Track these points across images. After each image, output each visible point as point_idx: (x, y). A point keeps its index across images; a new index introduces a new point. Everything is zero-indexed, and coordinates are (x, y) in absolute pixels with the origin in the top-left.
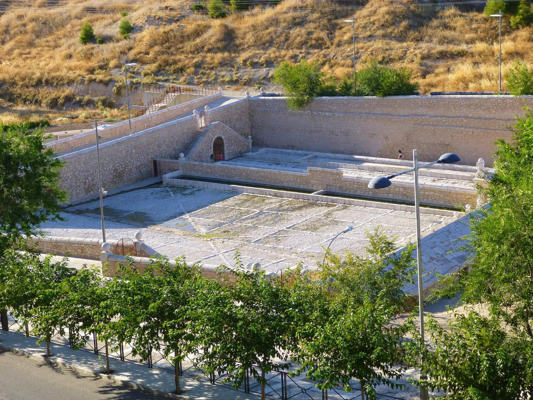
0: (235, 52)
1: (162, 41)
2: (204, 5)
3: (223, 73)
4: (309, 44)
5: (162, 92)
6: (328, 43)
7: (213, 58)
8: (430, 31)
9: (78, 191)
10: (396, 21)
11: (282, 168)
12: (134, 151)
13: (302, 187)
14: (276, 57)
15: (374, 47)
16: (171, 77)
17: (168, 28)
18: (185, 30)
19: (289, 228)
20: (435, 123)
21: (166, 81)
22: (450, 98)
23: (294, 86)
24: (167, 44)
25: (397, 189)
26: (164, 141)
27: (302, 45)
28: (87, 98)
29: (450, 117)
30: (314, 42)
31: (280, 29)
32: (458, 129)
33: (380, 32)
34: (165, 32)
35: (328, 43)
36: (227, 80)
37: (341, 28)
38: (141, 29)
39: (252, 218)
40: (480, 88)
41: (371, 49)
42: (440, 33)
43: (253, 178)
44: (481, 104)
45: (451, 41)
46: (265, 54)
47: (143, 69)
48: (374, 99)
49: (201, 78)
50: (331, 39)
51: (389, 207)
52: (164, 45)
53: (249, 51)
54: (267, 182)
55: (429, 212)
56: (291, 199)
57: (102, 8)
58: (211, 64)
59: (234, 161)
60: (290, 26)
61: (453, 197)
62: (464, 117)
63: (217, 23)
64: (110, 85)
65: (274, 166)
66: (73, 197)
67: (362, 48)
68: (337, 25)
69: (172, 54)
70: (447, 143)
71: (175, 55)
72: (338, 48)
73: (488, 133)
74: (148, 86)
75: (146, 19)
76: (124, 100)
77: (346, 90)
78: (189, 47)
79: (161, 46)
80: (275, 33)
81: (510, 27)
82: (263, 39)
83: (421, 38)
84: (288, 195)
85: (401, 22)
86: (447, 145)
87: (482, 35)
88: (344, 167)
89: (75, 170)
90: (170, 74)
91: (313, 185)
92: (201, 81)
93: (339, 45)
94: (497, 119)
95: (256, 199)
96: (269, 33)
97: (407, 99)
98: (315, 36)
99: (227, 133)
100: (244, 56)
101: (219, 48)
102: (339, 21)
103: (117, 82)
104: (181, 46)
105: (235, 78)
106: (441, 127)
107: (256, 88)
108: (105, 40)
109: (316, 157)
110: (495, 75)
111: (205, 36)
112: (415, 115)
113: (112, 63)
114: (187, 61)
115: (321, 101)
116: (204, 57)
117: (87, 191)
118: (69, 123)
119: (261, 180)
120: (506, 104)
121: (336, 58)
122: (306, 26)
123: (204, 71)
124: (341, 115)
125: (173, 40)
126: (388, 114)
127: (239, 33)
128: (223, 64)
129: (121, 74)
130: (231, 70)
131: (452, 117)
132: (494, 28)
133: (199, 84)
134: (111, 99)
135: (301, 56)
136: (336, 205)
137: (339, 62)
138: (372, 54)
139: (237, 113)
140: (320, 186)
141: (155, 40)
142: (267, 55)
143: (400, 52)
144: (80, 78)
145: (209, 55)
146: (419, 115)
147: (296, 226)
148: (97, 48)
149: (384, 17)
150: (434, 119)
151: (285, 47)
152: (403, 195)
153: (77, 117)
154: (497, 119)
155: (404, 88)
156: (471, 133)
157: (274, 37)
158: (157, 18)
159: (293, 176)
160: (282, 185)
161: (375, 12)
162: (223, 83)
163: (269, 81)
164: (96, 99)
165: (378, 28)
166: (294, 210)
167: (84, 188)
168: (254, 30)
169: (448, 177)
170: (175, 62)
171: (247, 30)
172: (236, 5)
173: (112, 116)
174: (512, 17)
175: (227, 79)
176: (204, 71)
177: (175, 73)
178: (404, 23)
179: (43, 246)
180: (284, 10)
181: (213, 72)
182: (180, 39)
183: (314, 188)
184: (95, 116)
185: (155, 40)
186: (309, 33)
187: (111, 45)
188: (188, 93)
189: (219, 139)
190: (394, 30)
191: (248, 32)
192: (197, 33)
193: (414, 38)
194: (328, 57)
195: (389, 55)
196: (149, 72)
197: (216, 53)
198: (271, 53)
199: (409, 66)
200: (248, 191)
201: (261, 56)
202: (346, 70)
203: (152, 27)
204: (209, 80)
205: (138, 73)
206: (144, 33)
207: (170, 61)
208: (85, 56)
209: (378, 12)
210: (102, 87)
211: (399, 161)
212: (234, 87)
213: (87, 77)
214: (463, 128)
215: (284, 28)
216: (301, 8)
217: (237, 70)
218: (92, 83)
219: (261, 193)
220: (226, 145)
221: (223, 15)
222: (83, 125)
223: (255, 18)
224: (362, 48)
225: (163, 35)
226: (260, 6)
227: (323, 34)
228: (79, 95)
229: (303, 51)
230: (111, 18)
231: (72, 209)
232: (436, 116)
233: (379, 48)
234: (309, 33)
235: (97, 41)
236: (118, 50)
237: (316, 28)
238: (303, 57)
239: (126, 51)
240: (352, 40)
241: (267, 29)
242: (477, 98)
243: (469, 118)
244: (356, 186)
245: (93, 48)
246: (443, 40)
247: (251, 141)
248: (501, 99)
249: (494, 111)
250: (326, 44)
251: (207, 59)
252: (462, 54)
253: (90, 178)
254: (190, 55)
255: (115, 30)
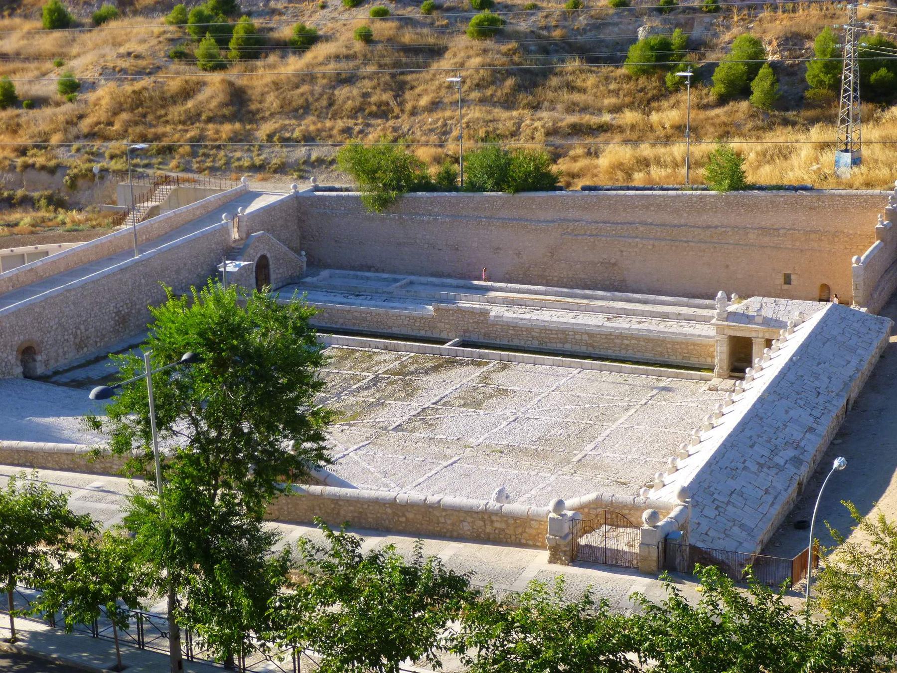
0: (251, 122)
1: (131, 106)
2: (186, 51)
3: (238, 154)
4: (367, 111)
5: (146, 184)
6: (397, 110)
7: (217, 132)
8: (550, 95)
9: (66, 349)
10: (496, 78)
11: (364, 302)
12: (143, 281)
13: (422, 333)
14: (318, 130)
15: (470, 116)
16: (154, 161)
17: (138, 85)
18: (166, 88)
19: (436, 403)
20: (594, 233)
21: (146, 166)
22: (617, 195)
23: (371, 175)
24: (140, 109)
25: (578, 337)
26: (185, 265)
27: (356, 112)
28: (20, 193)
29: (618, 223)
30: (374, 108)
31: (318, 89)
32: (630, 240)
33: (475, 95)
34: (134, 92)
35: (397, 110)
36: (246, 164)
37: (412, 88)
38: (93, 86)
39: (368, 388)
40: (650, 180)
41: (465, 120)
42: (566, 96)
43: (341, 321)
44: (666, 205)
45: (584, 109)
46: (300, 125)
47: (107, 147)
48: (500, 197)
49: (204, 162)
50: (401, 104)
51: (572, 365)
52: (136, 111)
53: (274, 120)
54: (364, 327)
55: (638, 371)
56: (412, 354)
57: (18, 54)
58: (216, 140)
59: (286, 292)
60: (333, 83)
61: (668, 348)
62: (639, 223)
63: (215, 78)
64: (58, 174)
65: (352, 299)
66: (60, 358)
67: (452, 118)
68: (404, 83)
69: (151, 126)
70: (613, 261)
71: (155, 126)
72: (413, 118)
73: (677, 246)
74: (122, 174)
75: (100, 71)
76: (82, 196)
77: (448, 183)
78: (176, 114)
79: (132, 112)
80: (312, 94)
81: (666, 89)
82: (294, 103)
83: (538, 104)
84: (407, 348)
85: (504, 80)
86: (614, 264)
87: (627, 100)
88: (464, 298)
89: (61, 315)
90: (151, 156)
91: (441, 331)
92: (204, 167)
93: (413, 113)
94: (691, 227)
95: (357, 355)
96: (302, 94)
97: (551, 197)
98: (374, 99)
99: (274, 248)
100: (266, 128)
101: (224, 116)
102: (409, 78)
103: (69, 168)
104: (163, 112)
105: (258, 161)
106: (604, 239)
107: (295, 177)
108: (36, 103)
109: (412, 283)
110: (669, 159)
111: (201, 97)
112: (564, 220)
113: (55, 139)
114: (177, 136)
115: (415, 198)
116: (203, 130)
117: (79, 347)
118: (8, 234)
119: (354, 324)
120: (706, 205)
121: (413, 133)
122: (359, 84)
123: (206, 151)
124: (447, 220)
125: (148, 103)
126: (522, 220)
127: (255, 94)
128: (235, 139)
129: (72, 156)
130: (249, 150)
131: (621, 223)
132: (642, 90)
133: (200, 171)
134: (62, 194)
135: (357, 129)
136: (488, 363)
137: (418, 138)
138: (468, 126)
139: (282, 218)
140: (453, 332)
141: (121, 104)
142: (303, 127)
143: (510, 124)
144: (7, 163)
145: (211, 126)
146: (569, 221)
147: (445, 400)
148: (25, 115)
149: (477, 71)
150: (594, 226)
151: (330, 116)
152: (587, 345)
153: (16, 225)
154: (691, 227)
155: (542, 181)
156: (650, 247)
157: (311, 99)
158: (117, 69)
159: (409, 317)
160: (389, 331)
161: (462, 65)
162: (240, 169)
163: (313, 166)
164: (36, 195)
165: (471, 89)
166: (427, 372)
167: (75, 343)
168: (277, 89)
169: (628, 313)
170: (157, 138)
171: (266, 89)
172: (239, 49)
173: (73, 222)
174: (669, 74)
175: (246, 163)
176: (206, 151)
177: (159, 154)
178: (510, 82)
179: (112, 463)
180: (320, 59)
181: (222, 153)
182: (160, 102)
183: (444, 335)
184: (44, 222)
185: (121, 104)
186: (365, 95)
187: (48, 111)
188: (192, 186)
189: (263, 258)
190: (496, 91)
191: (268, 93)
192: (187, 93)
193: (528, 104)
194: (400, 132)
195: (495, 130)
196: (118, 152)
197: (222, 123)
198: (309, 124)
199: (529, 146)
200: (340, 342)
201: (294, 129)
202: (433, 151)
203: (112, 85)
204: (217, 165)
205: (99, 155)
206: (100, 92)
207: (150, 136)
208: (7, 129)
209: (467, 64)
210: (44, 176)
211: (542, 288)
212: (259, 176)
213: (20, 161)
214: (638, 240)
215: (324, 87)
216: (347, 57)
217: (259, 150)
218: (28, 170)
219: (363, 345)
220: (272, 267)
221: (221, 67)
222: (33, 237)
223: (276, 72)
224: (452, 118)
225: (132, 96)
226: (278, 52)
227: (386, 97)
228: (7, 189)
229: (360, 121)
230: (38, 69)
231: (63, 379)
232: (596, 222)
233: (478, 119)
234: (365, 95)
235: (24, 105)
236: (61, 118)
237: (374, 88)
238: (361, 132)
239: (75, 120)
240: (435, 106)
241: (297, 87)
242: (660, 196)
243: (646, 224)
244: (511, 332)
245: (18, 116)
246: (571, 108)
247: (305, 259)
248: (696, 196)
249: (685, 215)
250: (393, 111)
251: (209, 133)
252: (605, 128)
253: (82, 327)
254: (180, 127)
255: (50, 87)
